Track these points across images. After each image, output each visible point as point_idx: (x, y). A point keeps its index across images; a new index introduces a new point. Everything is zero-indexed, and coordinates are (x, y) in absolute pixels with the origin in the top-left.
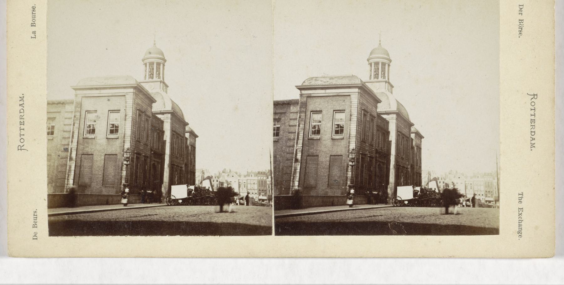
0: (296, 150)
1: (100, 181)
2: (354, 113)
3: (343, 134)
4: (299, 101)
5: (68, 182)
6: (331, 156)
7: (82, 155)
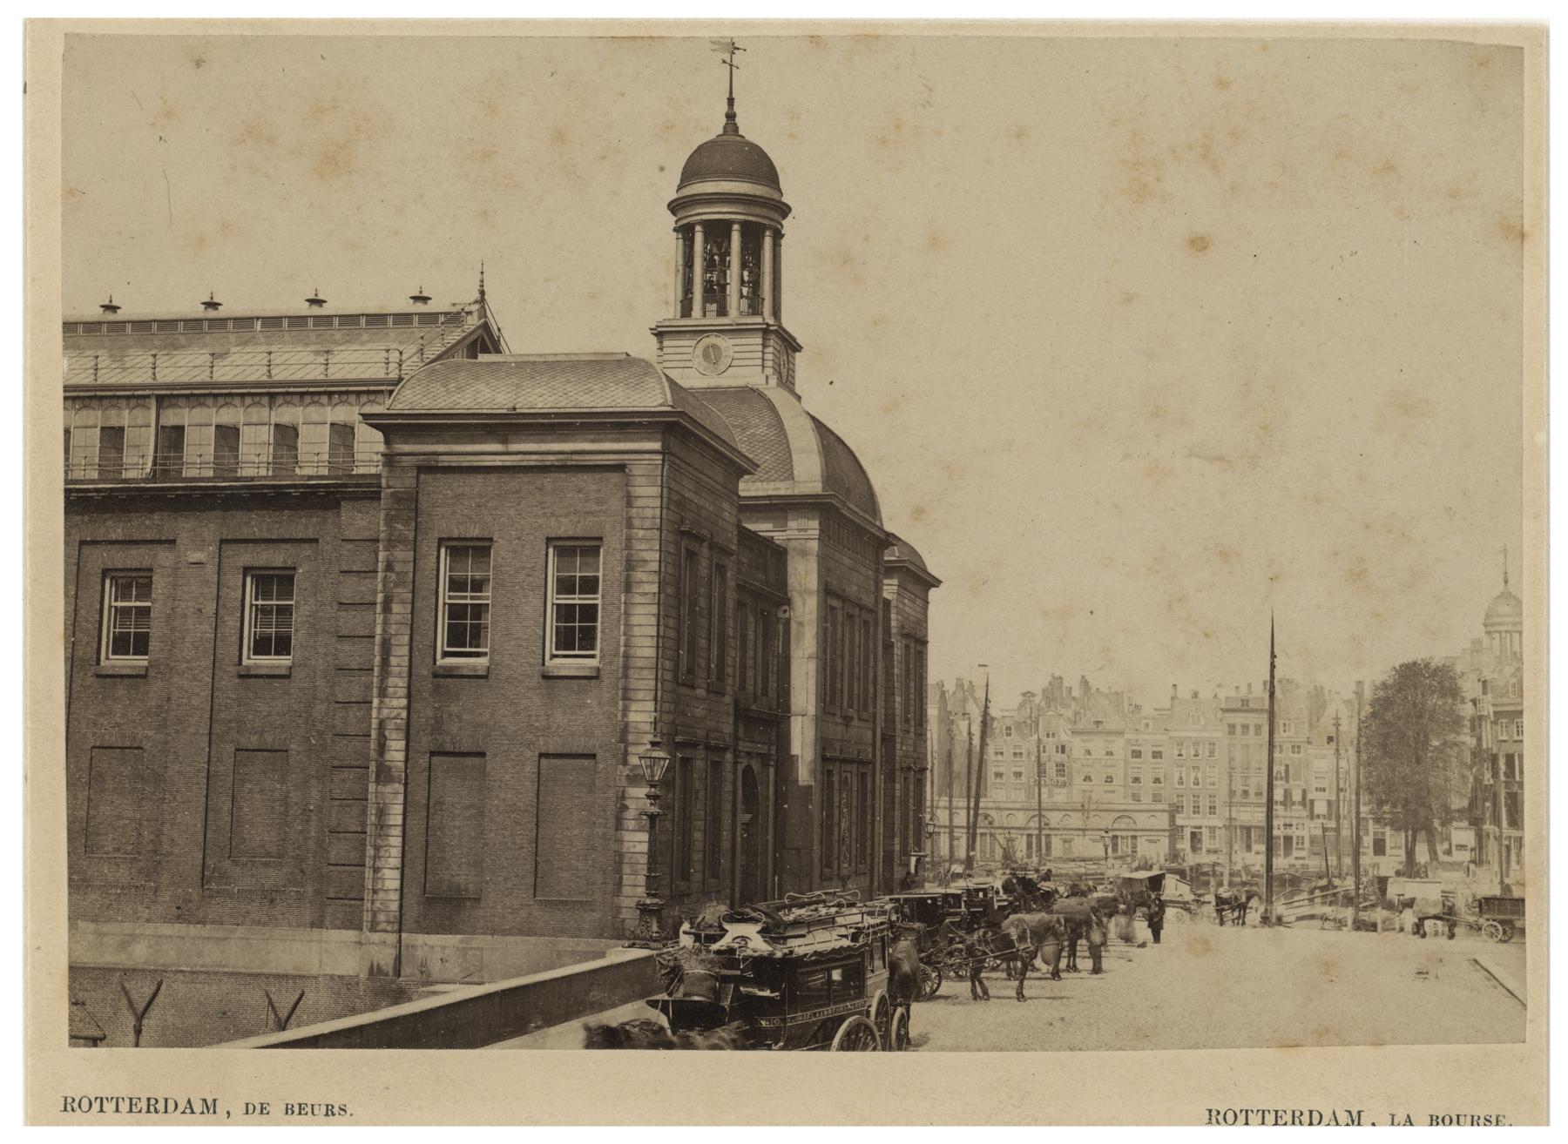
0: (382, 725)
1: (524, 877)
2: (646, 555)
3: (597, 652)
4: (379, 486)
5: (375, 880)
6: (541, 755)
7: (433, 754)
